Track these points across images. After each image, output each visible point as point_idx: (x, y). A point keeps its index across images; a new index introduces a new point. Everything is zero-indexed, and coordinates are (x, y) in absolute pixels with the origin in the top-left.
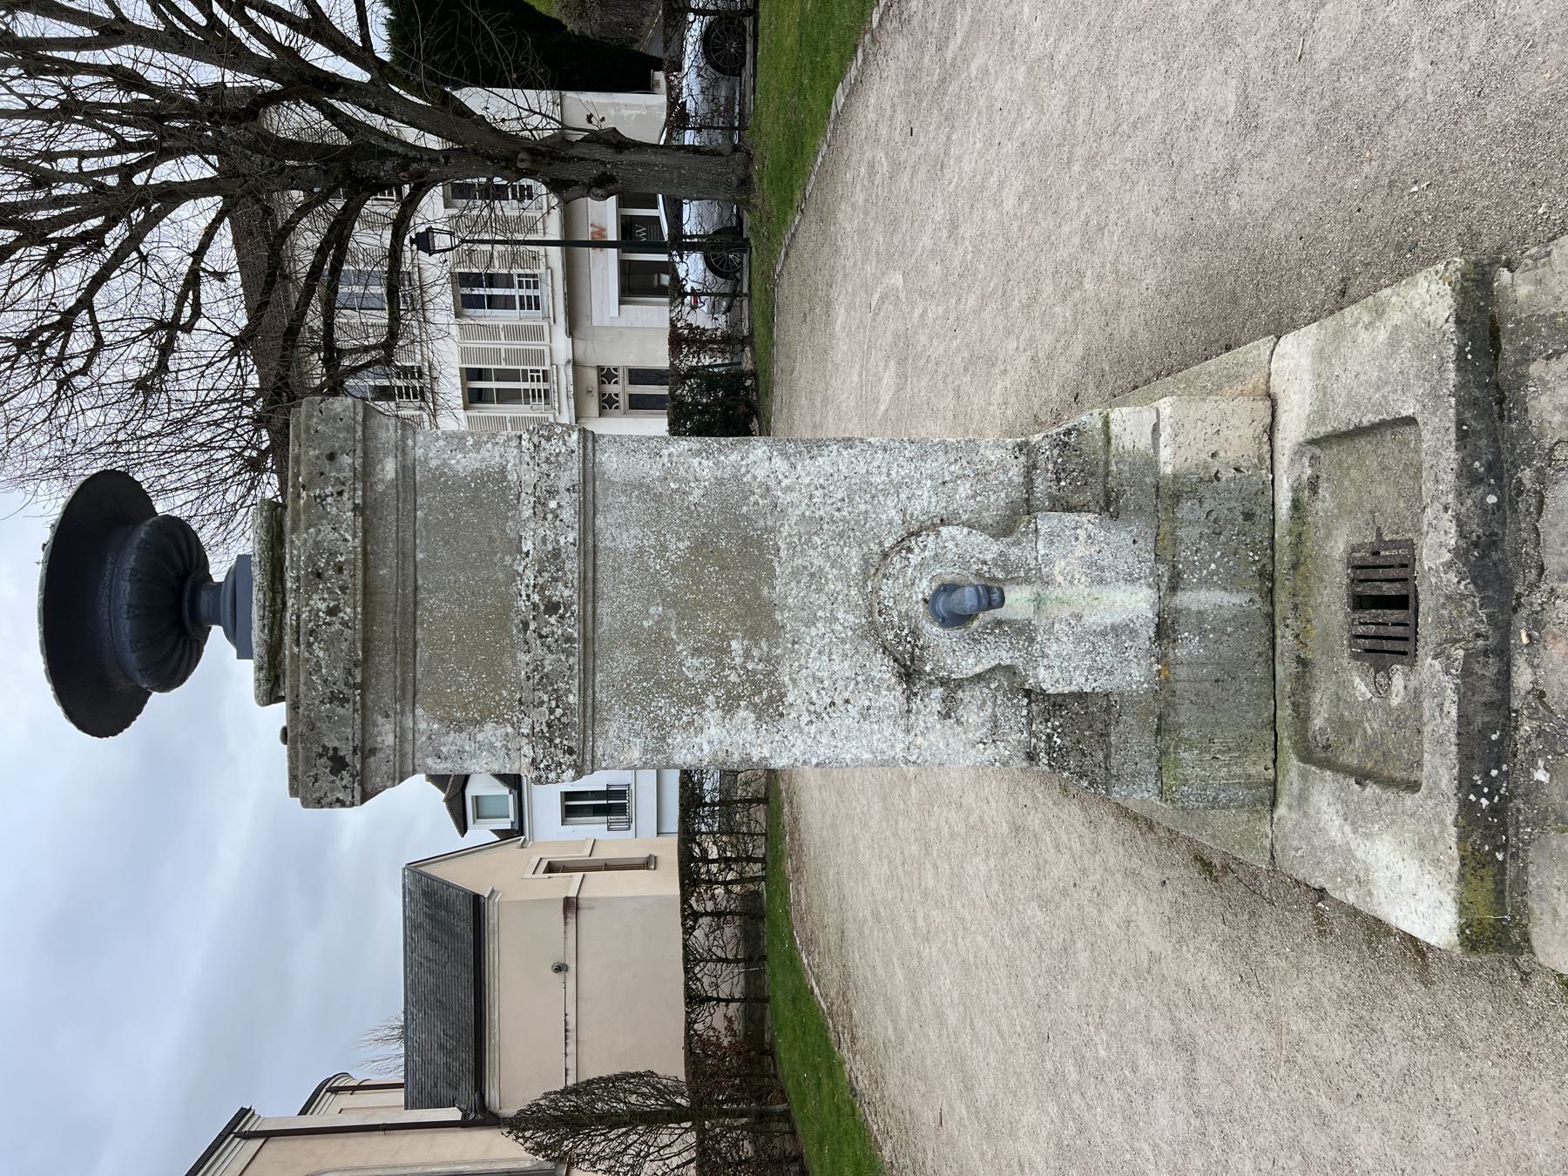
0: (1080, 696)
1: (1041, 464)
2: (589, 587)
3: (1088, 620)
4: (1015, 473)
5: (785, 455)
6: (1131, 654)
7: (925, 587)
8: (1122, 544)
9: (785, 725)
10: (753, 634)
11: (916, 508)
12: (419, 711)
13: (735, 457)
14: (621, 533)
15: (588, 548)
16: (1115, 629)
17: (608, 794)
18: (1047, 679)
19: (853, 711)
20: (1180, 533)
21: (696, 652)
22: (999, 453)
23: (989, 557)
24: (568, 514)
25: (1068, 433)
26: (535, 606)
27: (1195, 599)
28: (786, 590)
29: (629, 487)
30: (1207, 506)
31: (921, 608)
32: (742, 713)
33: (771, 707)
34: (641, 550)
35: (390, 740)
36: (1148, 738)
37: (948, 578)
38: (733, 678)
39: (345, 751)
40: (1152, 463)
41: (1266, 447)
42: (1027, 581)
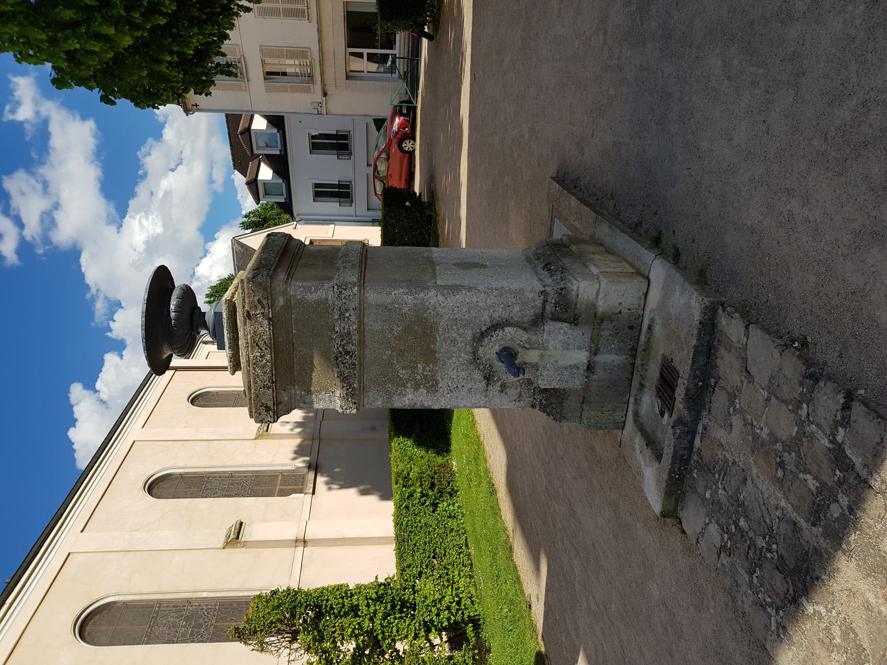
0: (554, 389)
1: (549, 300)
2: (362, 344)
3: (561, 363)
4: (539, 303)
5: (443, 295)
6: (576, 376)
7: (497, 348)
8: (579, 335)
9: (438, 394)
10: (427, 362)
11: (496, 315)
12: (297, 387)
13: (422, 295)
14: (374, 325)
15: (361, 330)
16: (571, 367)
17: (339, 186)
18: (542, 384)
19: (465, 390)
20: (602, 333)
21: (403, 368)
22: (533, 294)
23: (523, 339)
24: (353, 318)
25: (562, 289)
26: (341, 352)
27: (601, 358)
28: (442, 347)
29: (378, 306)
30: (614, 324)
31: (495, 356)
32: (421, 390)
33: (432, 387)
34: (383, 330)
35: (286, 399)
36: (579, 405)
37: (507, 345)
38: (418, 377)
39: (270, 404)
40: (594, 306)
41: (643, 301)
42: (538, 348)
